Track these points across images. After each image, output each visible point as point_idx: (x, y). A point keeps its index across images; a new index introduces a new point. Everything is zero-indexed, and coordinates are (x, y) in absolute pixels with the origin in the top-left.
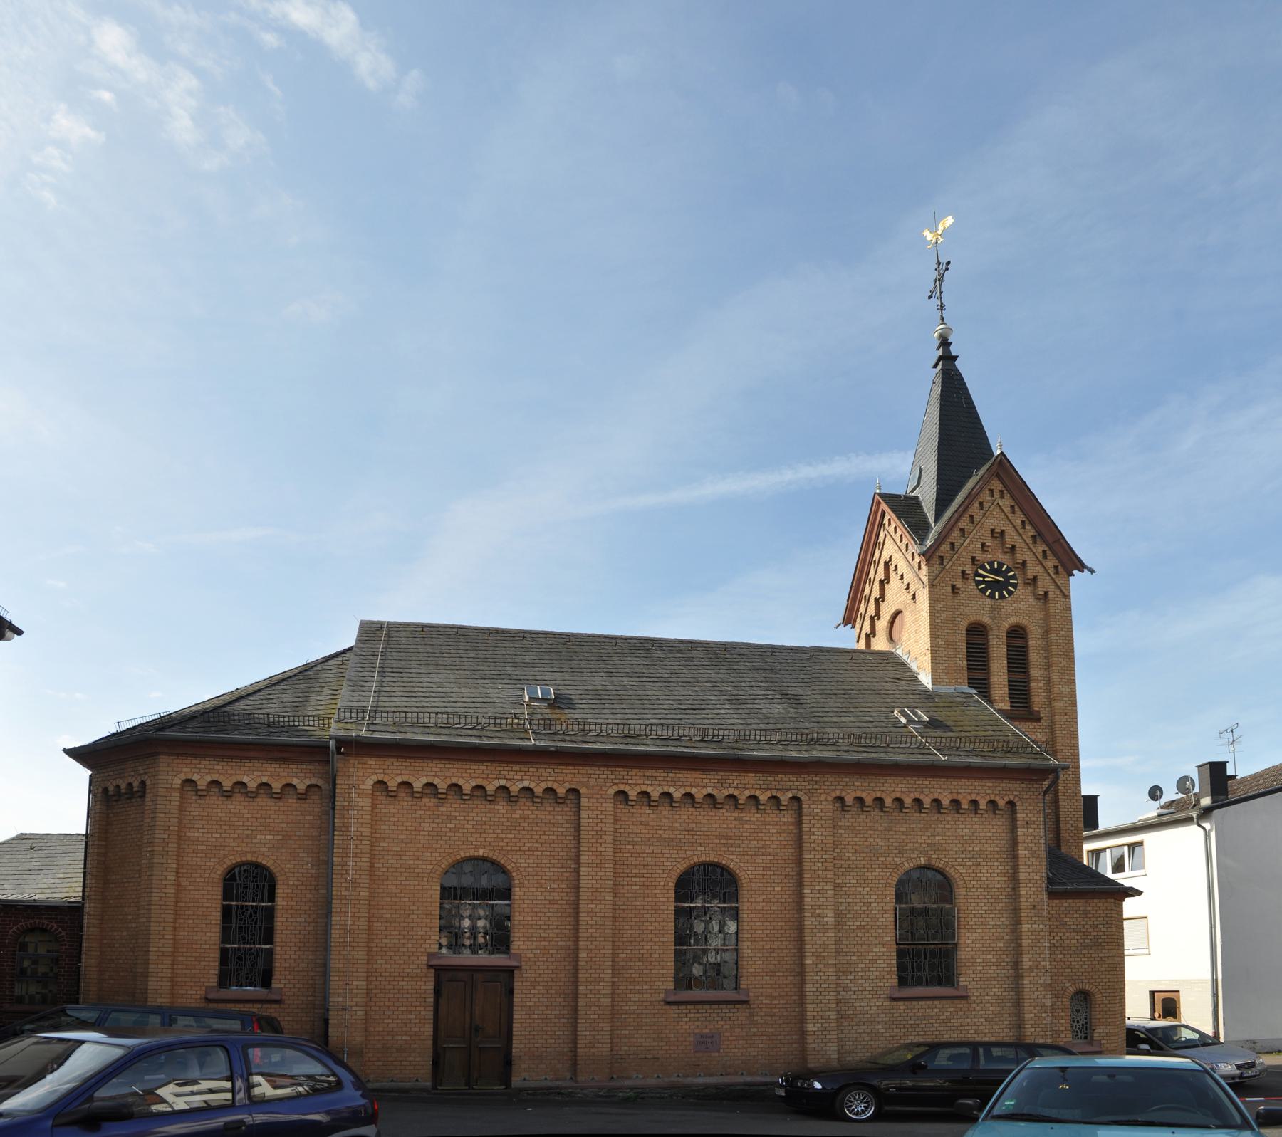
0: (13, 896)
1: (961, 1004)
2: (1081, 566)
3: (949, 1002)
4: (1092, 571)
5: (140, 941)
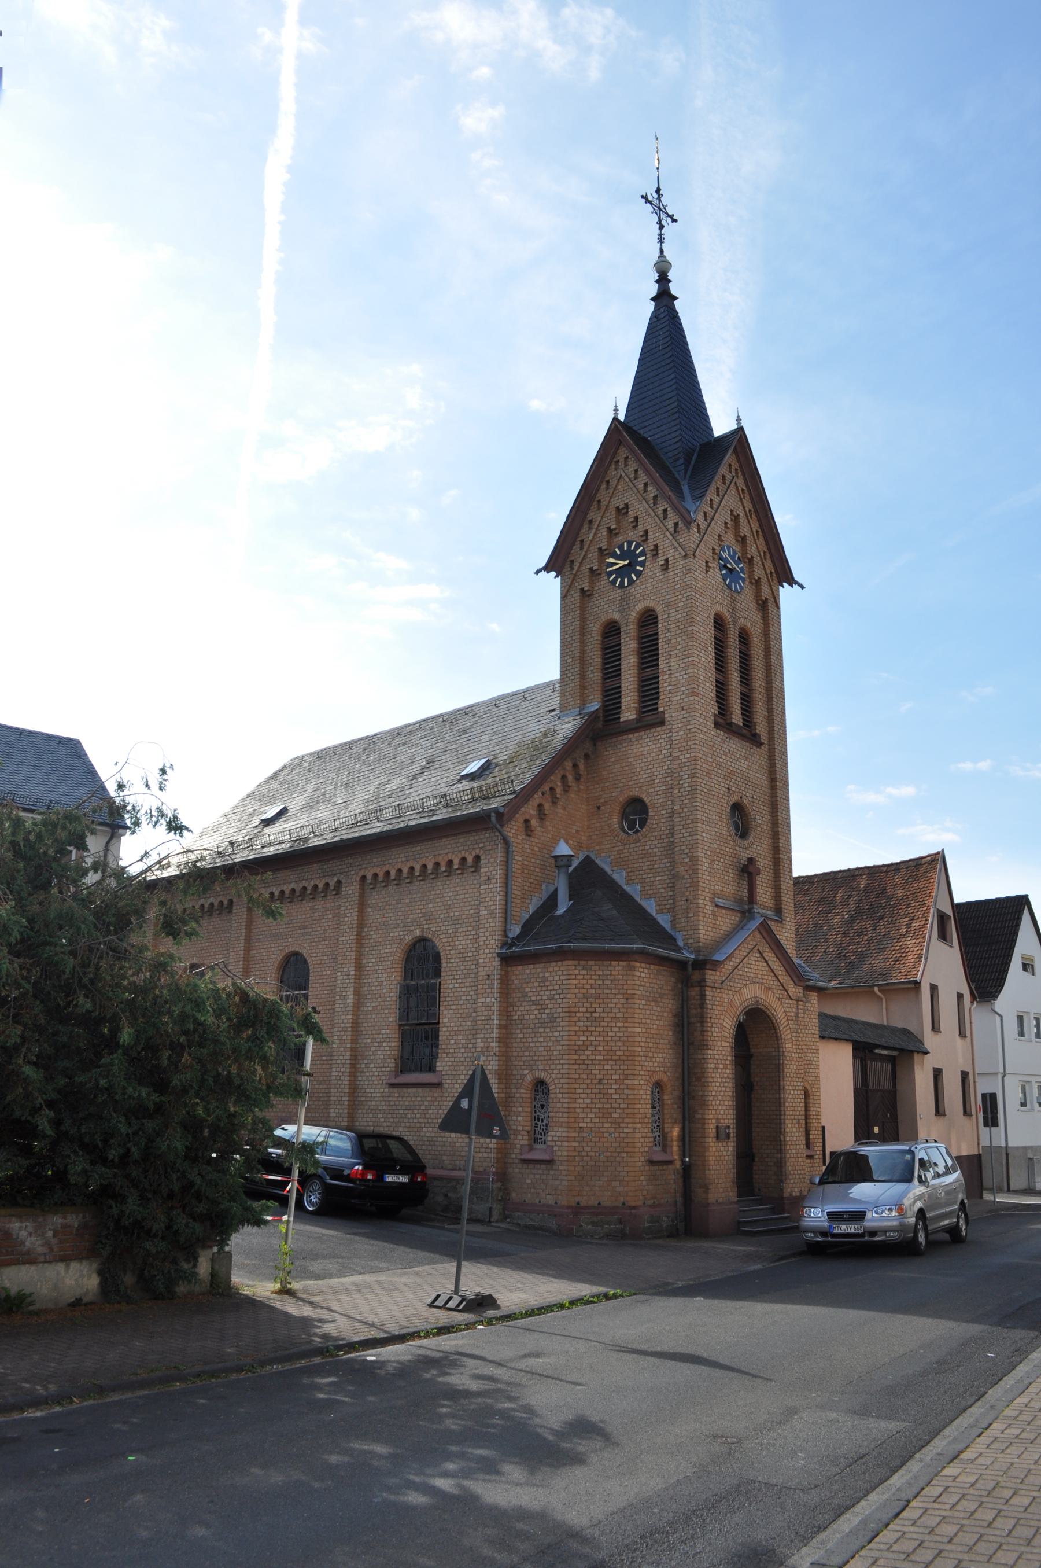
0: (265, 850)
1: (436, 1092)
2: (791, 581)
3: (427, 1090)
4: (802, 587)
5: (332, 1098)
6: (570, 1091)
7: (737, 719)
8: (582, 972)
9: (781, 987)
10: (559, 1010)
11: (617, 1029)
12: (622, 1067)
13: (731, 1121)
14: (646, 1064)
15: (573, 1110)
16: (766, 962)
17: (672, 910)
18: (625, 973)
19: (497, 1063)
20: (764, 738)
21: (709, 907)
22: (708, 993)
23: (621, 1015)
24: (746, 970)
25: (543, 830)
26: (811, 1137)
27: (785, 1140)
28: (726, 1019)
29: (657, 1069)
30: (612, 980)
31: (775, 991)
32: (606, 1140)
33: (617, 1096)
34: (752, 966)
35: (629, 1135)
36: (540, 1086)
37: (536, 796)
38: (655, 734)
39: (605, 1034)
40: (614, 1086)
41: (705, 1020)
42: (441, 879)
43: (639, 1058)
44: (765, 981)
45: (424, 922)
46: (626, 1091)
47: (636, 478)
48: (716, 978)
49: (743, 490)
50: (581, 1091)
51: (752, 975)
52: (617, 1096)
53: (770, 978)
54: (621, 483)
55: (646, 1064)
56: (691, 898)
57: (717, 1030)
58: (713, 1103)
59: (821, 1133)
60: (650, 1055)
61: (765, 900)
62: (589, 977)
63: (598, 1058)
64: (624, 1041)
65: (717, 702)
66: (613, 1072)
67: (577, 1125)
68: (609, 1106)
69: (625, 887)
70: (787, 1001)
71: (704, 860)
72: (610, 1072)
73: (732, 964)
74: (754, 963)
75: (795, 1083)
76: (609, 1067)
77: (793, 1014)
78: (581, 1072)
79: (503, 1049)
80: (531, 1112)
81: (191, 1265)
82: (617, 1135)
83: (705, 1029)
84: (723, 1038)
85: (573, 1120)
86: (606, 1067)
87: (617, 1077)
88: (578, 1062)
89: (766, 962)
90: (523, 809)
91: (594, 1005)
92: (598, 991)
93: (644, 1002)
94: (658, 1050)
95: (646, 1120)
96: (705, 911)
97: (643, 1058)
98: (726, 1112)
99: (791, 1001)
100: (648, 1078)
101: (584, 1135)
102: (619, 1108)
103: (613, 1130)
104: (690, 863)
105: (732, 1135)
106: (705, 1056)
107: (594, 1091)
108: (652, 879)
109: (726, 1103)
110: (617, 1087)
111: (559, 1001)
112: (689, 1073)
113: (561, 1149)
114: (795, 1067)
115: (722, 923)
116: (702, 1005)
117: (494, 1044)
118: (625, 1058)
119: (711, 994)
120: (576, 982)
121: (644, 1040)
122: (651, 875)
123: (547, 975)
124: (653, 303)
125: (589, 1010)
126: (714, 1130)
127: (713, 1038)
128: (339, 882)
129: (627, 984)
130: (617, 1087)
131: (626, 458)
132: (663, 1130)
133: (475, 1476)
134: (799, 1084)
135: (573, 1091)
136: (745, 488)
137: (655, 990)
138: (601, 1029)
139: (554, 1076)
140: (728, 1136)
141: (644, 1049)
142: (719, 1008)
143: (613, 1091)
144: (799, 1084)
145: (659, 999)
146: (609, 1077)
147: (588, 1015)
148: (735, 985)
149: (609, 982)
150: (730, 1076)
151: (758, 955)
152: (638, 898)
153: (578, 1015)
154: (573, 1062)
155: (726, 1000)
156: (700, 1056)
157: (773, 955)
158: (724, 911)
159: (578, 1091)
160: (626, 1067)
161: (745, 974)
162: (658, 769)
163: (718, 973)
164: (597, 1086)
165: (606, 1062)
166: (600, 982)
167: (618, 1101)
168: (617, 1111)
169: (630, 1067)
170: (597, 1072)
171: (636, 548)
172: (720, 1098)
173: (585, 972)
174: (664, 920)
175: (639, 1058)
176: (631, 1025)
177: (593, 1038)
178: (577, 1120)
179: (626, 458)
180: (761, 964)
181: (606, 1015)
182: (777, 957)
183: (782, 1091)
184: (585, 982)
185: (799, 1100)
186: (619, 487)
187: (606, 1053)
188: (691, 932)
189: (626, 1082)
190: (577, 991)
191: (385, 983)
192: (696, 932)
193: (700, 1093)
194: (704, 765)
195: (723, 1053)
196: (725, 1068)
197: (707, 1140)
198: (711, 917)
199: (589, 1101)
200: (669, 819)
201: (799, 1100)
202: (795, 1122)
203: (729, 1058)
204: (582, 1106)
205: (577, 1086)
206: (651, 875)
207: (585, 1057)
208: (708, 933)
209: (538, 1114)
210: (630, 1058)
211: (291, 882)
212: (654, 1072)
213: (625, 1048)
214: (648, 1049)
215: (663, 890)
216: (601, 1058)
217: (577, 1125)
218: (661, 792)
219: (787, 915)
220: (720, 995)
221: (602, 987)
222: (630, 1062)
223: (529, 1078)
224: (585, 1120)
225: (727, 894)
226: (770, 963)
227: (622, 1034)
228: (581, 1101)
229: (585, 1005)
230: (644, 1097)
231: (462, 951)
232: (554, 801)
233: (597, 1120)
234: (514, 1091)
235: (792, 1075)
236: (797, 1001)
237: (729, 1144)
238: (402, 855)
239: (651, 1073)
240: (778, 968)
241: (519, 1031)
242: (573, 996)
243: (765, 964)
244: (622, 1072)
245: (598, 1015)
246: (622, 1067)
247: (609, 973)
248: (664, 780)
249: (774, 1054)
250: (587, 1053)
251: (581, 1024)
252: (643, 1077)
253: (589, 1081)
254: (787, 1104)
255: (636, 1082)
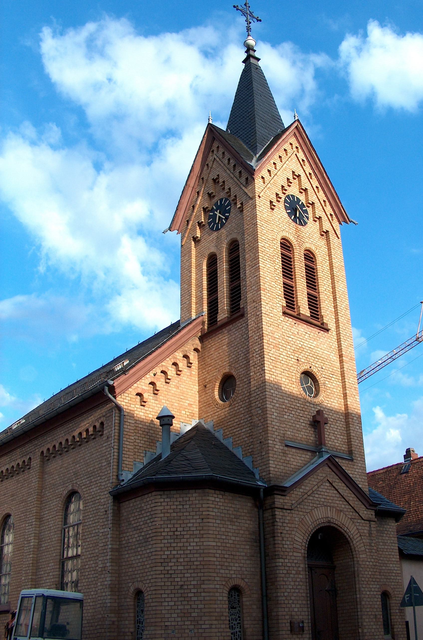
6: (157, 596)
7: (305, 310)
8: (166, 500)
9: (352, 510)
10: (150, 532)
11: (195, 544)
12: (199, 575)
13: (305, 617)
14: (222, 571)
15: (159, 612)
16: (337, 490)
17: (252, 454)
18: (200, 498)
19: (110, 579)
20: (332, 325)
21: (279, 447)
22: (278, 513)
23: (198, 532)
24: (317, 496)
25: (157, 402)
26: (395, 630)
27: (362, 632)
28: (297, 534)
29: (234, 576)
30: (190, 505)
31: (347, 513)
32: (186, 635)
33: (196, 599)
34: (322, 493)
35: (207, 631)
36: (139, 593)
37: (147, 376)
38: (239, 325)
39: (185, 548)
40: (193, 591)
41: (276, 535)
42: (84, 445)
43: (214, 567)
44: (336, 505)
45: (74, 479)
46: (203, 594)
47: (223, 158)
48: (286, 501)
49: (331, 215)
50: (166, 596)
51: (323, 500)
52: (196, 599)
53: (341, 502)
54: (215, 163)
55: (222, 571)
56: (263, 440)
57: (288, 543)
58: (286, 602)
59: (405, 626)
60: (226, 564)
61: (337, 444)
62: (172, 503)
63: (180, 568)
64: (200, 553)
65: (285, 298)
66: (192, 579)
67: (163, 624)
68: (188, 607)
69: (222, 441)
70: (359, 521)
71: (273, 410)
72: (189, 579)
73: (301, 490)
74: (324, 490)
75: (371, 586)
76: (188, 575)
77: (366, 531)
78: (166, 580)
79: (116, 568)
80: (135, 617)
81: (47, 636)
82: (196, 631)
83: (276, 542)
84: (295, 550)
85: (160, 620)
86: (186, 575)
87: (195, 583)
88: (163, 572)
89: (337, 490)
90: (135, 385)
91: (176, 526)
92: (179, 514)
93: (218, 521)
94: (234, 561)
95: (223, 618)
96: (275, 449)
97: (219, 567)
98: (300, 610)
99: (363, 521)
100: (224, 583)
101: (169, 632)
102: (198, 608)
103: (193, 627)
104: (262, 414)
105: (306, 628)
106: (277, 564)
107: (176, 595)
108: (240, 432)
109: (300, 602)
110: (195, 591)
111: (150, 524)
112: (266, 580)
113: (214, 536)
114: (370, 573)
115: (292, 460)
116: (273, 523)
117: (108, 564)
118: (202, 567)
119: (281, 514)
120: (162, 508)
121: (219, 552)
122: (239, 429)
123: (143, 505)
124: (244, 64)
125: (172, 530)
126: (288, 625)
127: (284, 550)
128: (30, 459)
129: (202, 507)
130: (195, 591)
131: (218, 147)
132: (243, 627)
133: (80, 426)
134: (374, 586)
135: (160, 596)
136: (305, 159)
137: (231, 512)
138: (181, 545)
139: (147, 585)
140: (302, 629)
141: (219, 559)
142: (289, 525)
143: (192, 595)
144: (374, 586)
145: (235, 520)
146: (189, 583)
147: (172, 533)
148: (306, 507)
149: (188, 506)
150: (303, 580)
151: (328, 484)
152: (231, 449)
153: (164, 534)
154: (160, 572)
155: (297, 519)
156: (273, 565)
157: (343, 485)
158: (294, 450)
159: (164, 596)
160: (202, 574)
161: (316, 499)
162: (241, 349)
163: (288, 498)
164: (179, 591)
165: (186, 571)
166: (181, 507)
167: (196, 603)
168: (196, 611)
169: (206, 574)
170: (179, 579)
171: (225, 202)
172: (293, 598)
173: (169, 500)
174: (247, 462)
175: (214, 567)
176: (206, 539)
177: (175, 552)
178: (163, 620)
179: (218, 147)
180: (331, 492)
181: (185, 533)
182: (347, 487)
183: (358, 593)
184: (168, 507)
185: (376, 599)
186: (214, 166)
187: (186, 564)
188: (264, 467)
189: (203, 586)
190: (162, 515)
191: (52, 528)
192: (267, 466)
193: (275, 595)
194: (335, 415)
195: (296, 561)
196: (298, 573)
197: (281, 633)
198: (281, 454)
199: (173, 603)
200: (43, 508)
201: (376, 599)
202: (372, 617)
203: (302, 566)
204: (167, 608)
205: (163, 592)
206: (239, 429)
207: (169, 568)
208: (278, 467)
209: (140, 617)
210: (206, 567)
211: (6, 465)
212: (231, 578)
213: (201, 559)
214: (225, 560)
215: (246, 439)
216: (181, 568)
217: (163, 624)
218: (243, 366)
219: (357, 456)
220: (291, 515)
221: (182, 510)
222: (206, 570)
223: (132, 589)
224: (170, 620)
225: (298, 438)
226: (339, 490)
227: (198, 548)
228: (166, 604)
229: (169, 526)
230: (221, 598)
231: (94, 496)
232: (167, 381)
233: (179, 619)
234: (123, 600)
235: (367, 579)
236: (370, 521)
237: (304, 636)
238: (62, 432)
239: (226, 579)
240: (349, 495)
241: (126, 553)
242: (160, 519)
243: (336, 492)
244: (199, 578)
245: (179, 533)
246: (199, 575)
247: (187, 499)
248: (245, 356)
249: (350, 563)
250: (170, 564)
251: (166, 541)
252: (219, 583)
253: (173, 588)
254: (363, 603)
255: (211, 586)
